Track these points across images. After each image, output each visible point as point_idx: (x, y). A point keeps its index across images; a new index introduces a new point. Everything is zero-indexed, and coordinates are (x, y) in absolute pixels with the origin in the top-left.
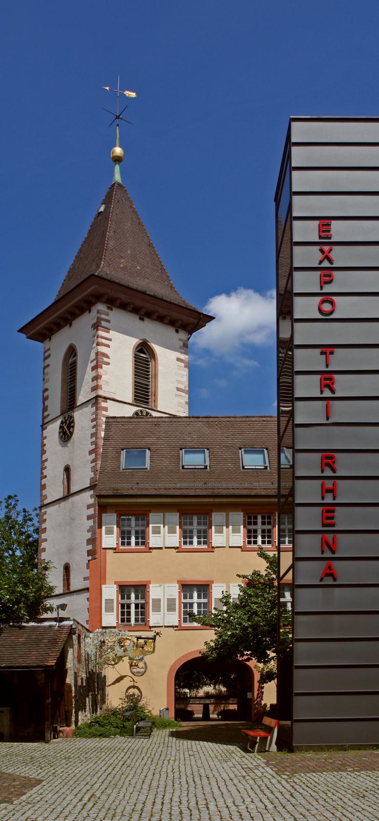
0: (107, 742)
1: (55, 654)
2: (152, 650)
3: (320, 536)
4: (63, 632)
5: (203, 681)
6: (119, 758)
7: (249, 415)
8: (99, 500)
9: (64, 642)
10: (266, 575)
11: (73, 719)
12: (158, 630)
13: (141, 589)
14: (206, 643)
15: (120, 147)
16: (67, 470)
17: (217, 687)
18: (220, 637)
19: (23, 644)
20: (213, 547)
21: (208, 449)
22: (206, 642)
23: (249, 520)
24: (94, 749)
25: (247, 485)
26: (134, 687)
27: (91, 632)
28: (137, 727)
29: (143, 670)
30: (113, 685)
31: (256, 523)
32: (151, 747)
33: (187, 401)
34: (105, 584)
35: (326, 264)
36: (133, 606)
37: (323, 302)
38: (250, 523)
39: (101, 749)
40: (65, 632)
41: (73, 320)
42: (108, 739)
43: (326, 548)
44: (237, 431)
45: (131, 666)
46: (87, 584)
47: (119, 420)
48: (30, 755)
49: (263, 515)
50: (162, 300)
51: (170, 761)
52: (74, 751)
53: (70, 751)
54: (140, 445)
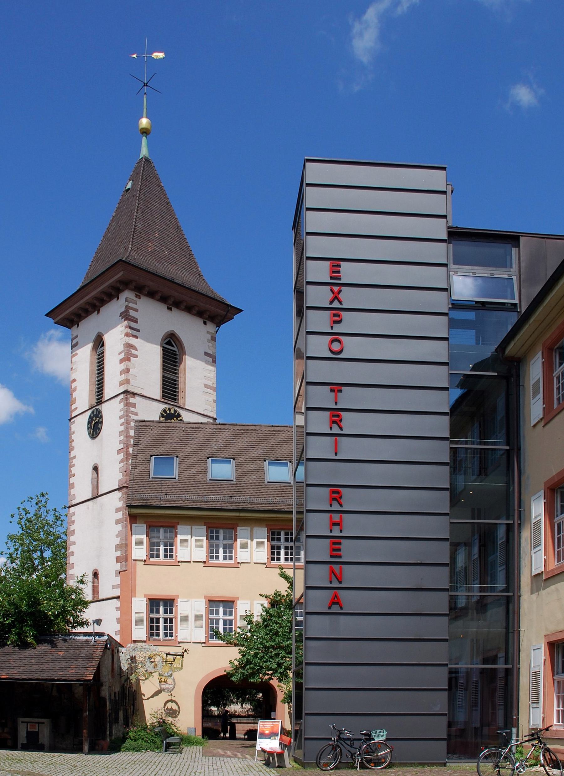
0: (140, 756)
1: (92, 669)
2: (180, 666)
3: (327, 567)
4: (99, 647)
5: (231, 699)
6: (152, 770)
7: (274, 425)
8: (129, 510)
9: (100, 657)
10: (287, 595)
11: (108, 733)
12: (185, 646)
13: (169, 603)
14: (231, 662)
15: (147, 117)
16: (96, 469)
17: (244, 705)
18: (244, 656)
19: (63, 657)
20: (238, 563)
21: (234, 459)
22: (231, 661)
23: (273, 537)
24: (128, 762)
25: (270, 500)
26: (172, 701)
27: (123, 647)
28: (167, 743)
29: (172, 686)
30: (151, 699)
31: (279, 540)
32: (180, 762)
33: (215, 399)
34: (135, 597)
35: (336, 304)
36: (161, 620)
37: (332, 341)
38: (273, 539)
39: (135, 762)
40: (101, 647)
41: (102, 306)
42: (140, 753)
43: (334, 577)
44: (262, 441)
45: (160, 682)
46: (117, 593)
47: (148, 424)
48: (72, 764)
49: (286, 531)
50: (189, 289)
51: (197, 773)
52: (111, 762)
53: (107, 762)
54: (168, 451)
